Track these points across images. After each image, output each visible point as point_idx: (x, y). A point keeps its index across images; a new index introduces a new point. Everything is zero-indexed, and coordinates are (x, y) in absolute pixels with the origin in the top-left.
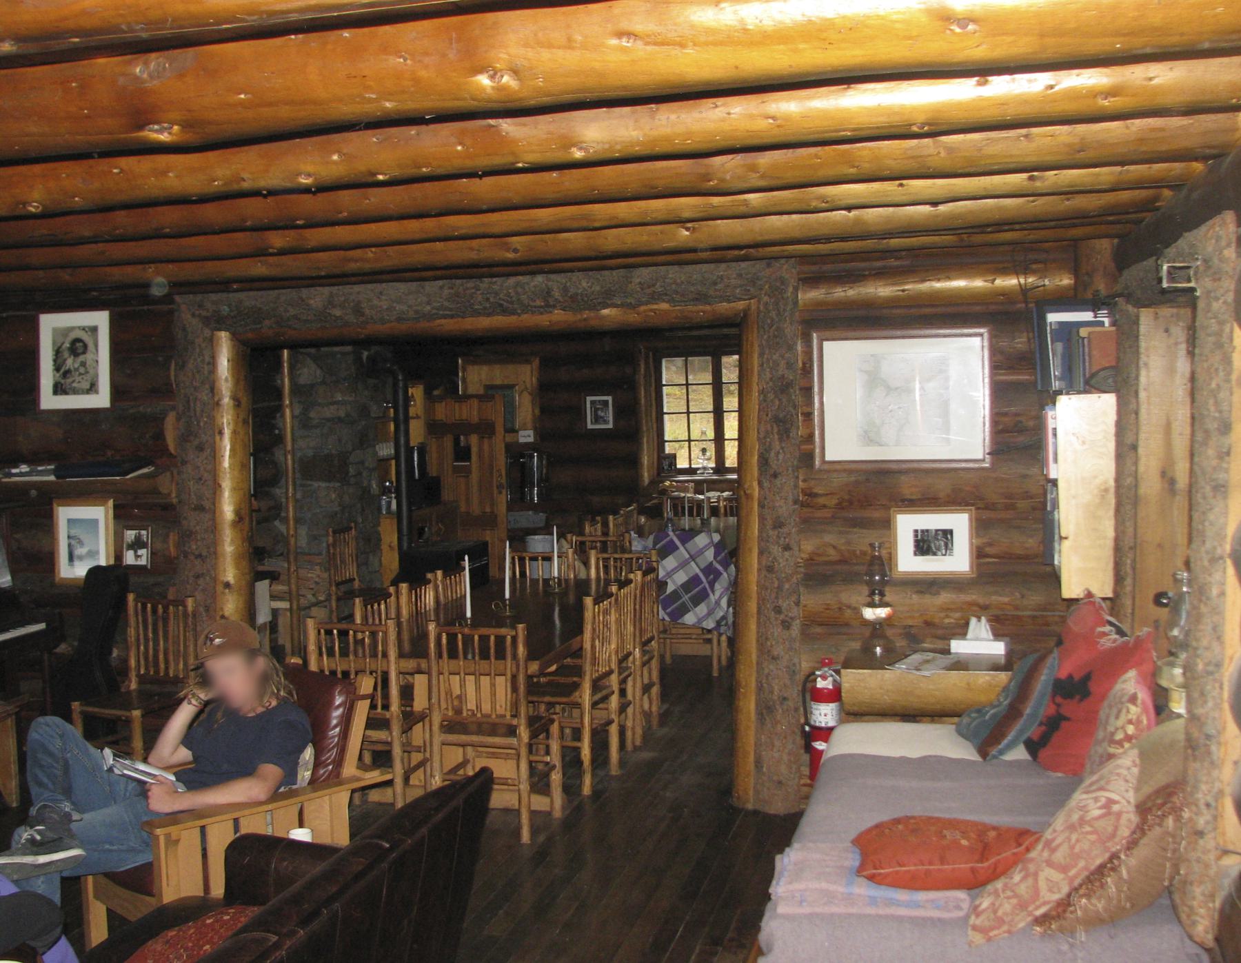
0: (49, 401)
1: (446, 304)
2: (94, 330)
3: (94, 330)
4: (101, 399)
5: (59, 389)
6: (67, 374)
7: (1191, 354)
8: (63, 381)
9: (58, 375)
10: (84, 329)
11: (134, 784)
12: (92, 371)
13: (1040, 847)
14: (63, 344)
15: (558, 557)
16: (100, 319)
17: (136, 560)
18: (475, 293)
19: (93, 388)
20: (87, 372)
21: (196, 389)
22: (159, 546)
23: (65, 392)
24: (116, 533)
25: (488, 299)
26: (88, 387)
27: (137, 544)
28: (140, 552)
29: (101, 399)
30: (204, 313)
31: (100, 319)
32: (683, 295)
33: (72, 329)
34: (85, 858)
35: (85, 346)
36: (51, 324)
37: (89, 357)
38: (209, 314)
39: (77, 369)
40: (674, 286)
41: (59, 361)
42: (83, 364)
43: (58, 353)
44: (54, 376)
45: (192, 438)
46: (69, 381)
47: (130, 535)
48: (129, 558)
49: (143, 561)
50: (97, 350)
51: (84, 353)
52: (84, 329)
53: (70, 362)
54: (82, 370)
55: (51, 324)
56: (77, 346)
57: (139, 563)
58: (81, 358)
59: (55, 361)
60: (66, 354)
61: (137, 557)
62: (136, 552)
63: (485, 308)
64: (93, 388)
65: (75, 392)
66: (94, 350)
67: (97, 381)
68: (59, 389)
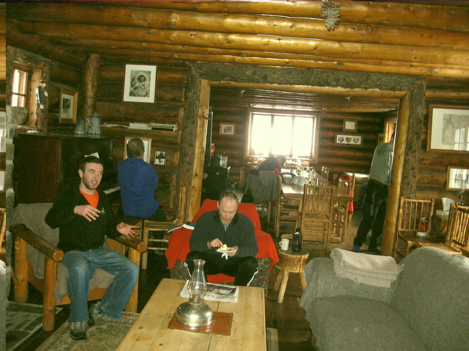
0: (127, 98)
1: (299, 79)
2: (149, 73)
3: (149, 73)
4: (151, 99)
5: (132, 94)
6: (136, 89)
7: (116, 257)
8: (134, 91)
9: (132, 88)
10: (145, 72)
11: (158, 251)
12: (147, 89)
13: (135, 8)
14: (136, 76)
15: (63, 107)
16: (153, 69)
17: (160, 163)
18: (311, 77)
19: (147, 95)
20: (145, 89)
21: (194, 100)
22: (169, 157)
23: (135, 95)
24: (152, 152)
25: (316, 80)
26: (145, 94)
27: (161, 157)
28: (161, 160)
29: (151, 99)
30: (201, 72)
31: (153, 69)
32: (386, 86)
33: (140, 71)
34: (63, 309)
35: (145, 79)
36: (130, 69)
37: (146, 82)
38: (203, 72)
39: (140, 87)
40: (384, 83)
41: (133, 83)
42: (144, 85)
43: (133, 80)
44: (130, 89)
45: (191, 118)
46: (137, 91)
47: (158, 153)
48: (157, 162)
49: (163, 163)
50: (150, 80)
51: (144, 81)
52: (145, 72)
53: (138, 84)
54: (143, 87)
55: (130, 69)
56: (141, 79)
57: (161, 164)
58: (143, 83)
59: (131, 83)
60: (136, 81)
61: (160, 161)
62: (160, 160)
63: (313, 83)
64: (147, 95)
65: (139, 96)
66: (148, 80)
67: (149, 92)
68: (132, 94)
